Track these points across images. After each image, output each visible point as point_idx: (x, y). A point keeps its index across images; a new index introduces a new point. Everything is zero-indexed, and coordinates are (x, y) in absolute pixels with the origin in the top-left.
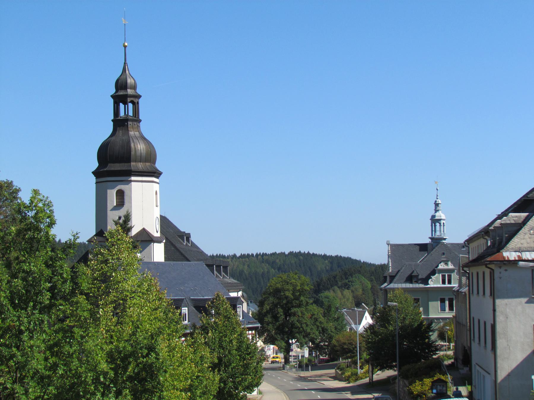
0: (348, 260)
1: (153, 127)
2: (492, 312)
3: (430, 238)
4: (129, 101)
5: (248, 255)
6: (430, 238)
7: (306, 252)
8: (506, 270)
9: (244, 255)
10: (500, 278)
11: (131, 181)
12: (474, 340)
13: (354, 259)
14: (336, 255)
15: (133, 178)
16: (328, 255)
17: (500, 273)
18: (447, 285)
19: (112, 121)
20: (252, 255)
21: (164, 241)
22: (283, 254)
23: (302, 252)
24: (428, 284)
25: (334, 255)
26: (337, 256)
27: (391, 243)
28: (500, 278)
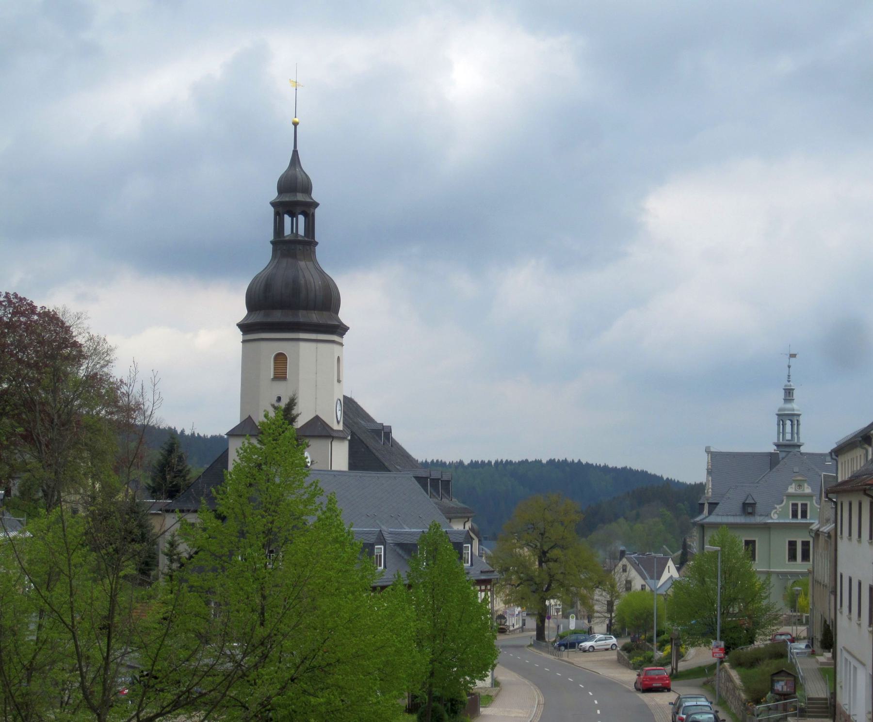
5: (483, 462)
7: (576, 461)
9: (477, 462)
13: (653, 473)
14: (623, 466)
16: (610, 466)
19: (272, 242)
20: (490, 462)
23: (569, 460)
27: (712, 450)
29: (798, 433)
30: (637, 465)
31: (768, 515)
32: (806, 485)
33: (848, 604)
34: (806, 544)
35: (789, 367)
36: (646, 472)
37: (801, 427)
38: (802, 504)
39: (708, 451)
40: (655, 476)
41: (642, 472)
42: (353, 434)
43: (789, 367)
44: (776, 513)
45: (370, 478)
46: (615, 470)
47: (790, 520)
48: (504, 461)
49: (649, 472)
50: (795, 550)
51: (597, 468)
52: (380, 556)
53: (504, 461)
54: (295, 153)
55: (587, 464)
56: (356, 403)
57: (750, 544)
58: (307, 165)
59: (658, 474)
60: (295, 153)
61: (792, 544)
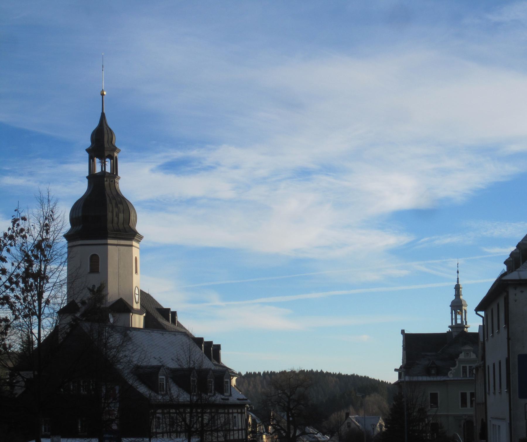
0: (366, 379)
1: (134, 180)
2: (506, 340)
3: (450, 327)
4: (106, 155)
5: (255, 373)
6: (450, 327)
7: (319, 371)
8: (522, 292)
9: (250, 373)
10: (516, 301)
11: (107, 244)
12: (489, 394)
13: (372, 378)
14: (352, 373)
15: (110, 241)
16: (343, 374)
17: (515, 295)
18: (468, 377)
19: (87, 177)
20: (259, 373)
21: (144, 315)
22: (293, 372)
23: (315, 370)
24: (448, 377)
25: (349, 374)
26: (353, 376)
27: (406, 332)
28: (516, 301)
29: (465, 319)
30: (361, 373)
31: (446, 374)
32: (472, 353)
33: (493, 384)
34: (472, 395)
35: (458, 272)
36: (368, 377)
37: (467, 314)
38: (469, 367)
39: (403, 332)
40: (374, 380)
41: (365, 377)
42: (148, 313)
43: (458, 272)
44: (451, 373)
45: (156, 335)
46: (346, 376)
47: (461, 377)
48: (269, 372)
49: (370, 377)
50: (466, 400)
51: (334, 375)
52: (163, 384)
53: (269, 372)
54: (103, 116)
55: (327, 373)
56: (152, 298)
57: (434, 397)
58: (110, 122)
59: (376, 378)
60: (103, 116)
61: (464, 396)
